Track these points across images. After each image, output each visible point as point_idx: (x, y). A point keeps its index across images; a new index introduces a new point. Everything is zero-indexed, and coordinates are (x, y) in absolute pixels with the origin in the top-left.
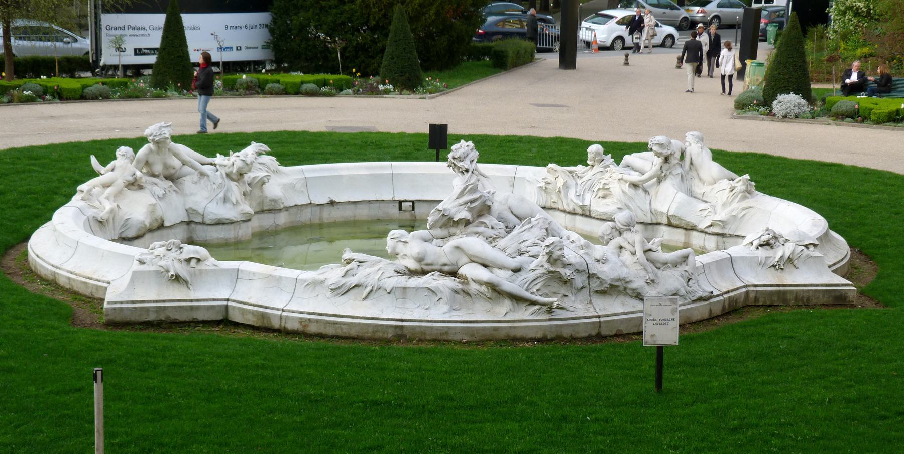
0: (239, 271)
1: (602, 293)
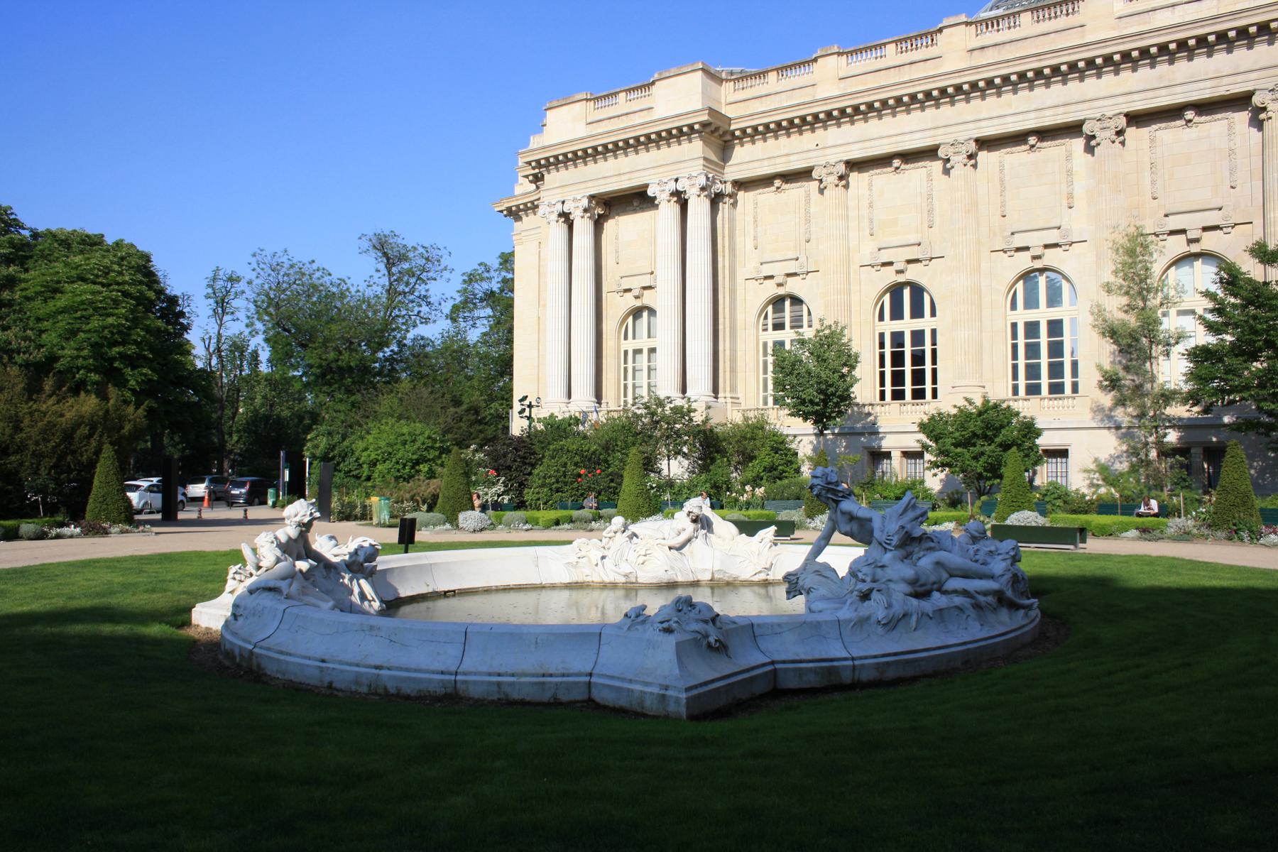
0: (755, 627)
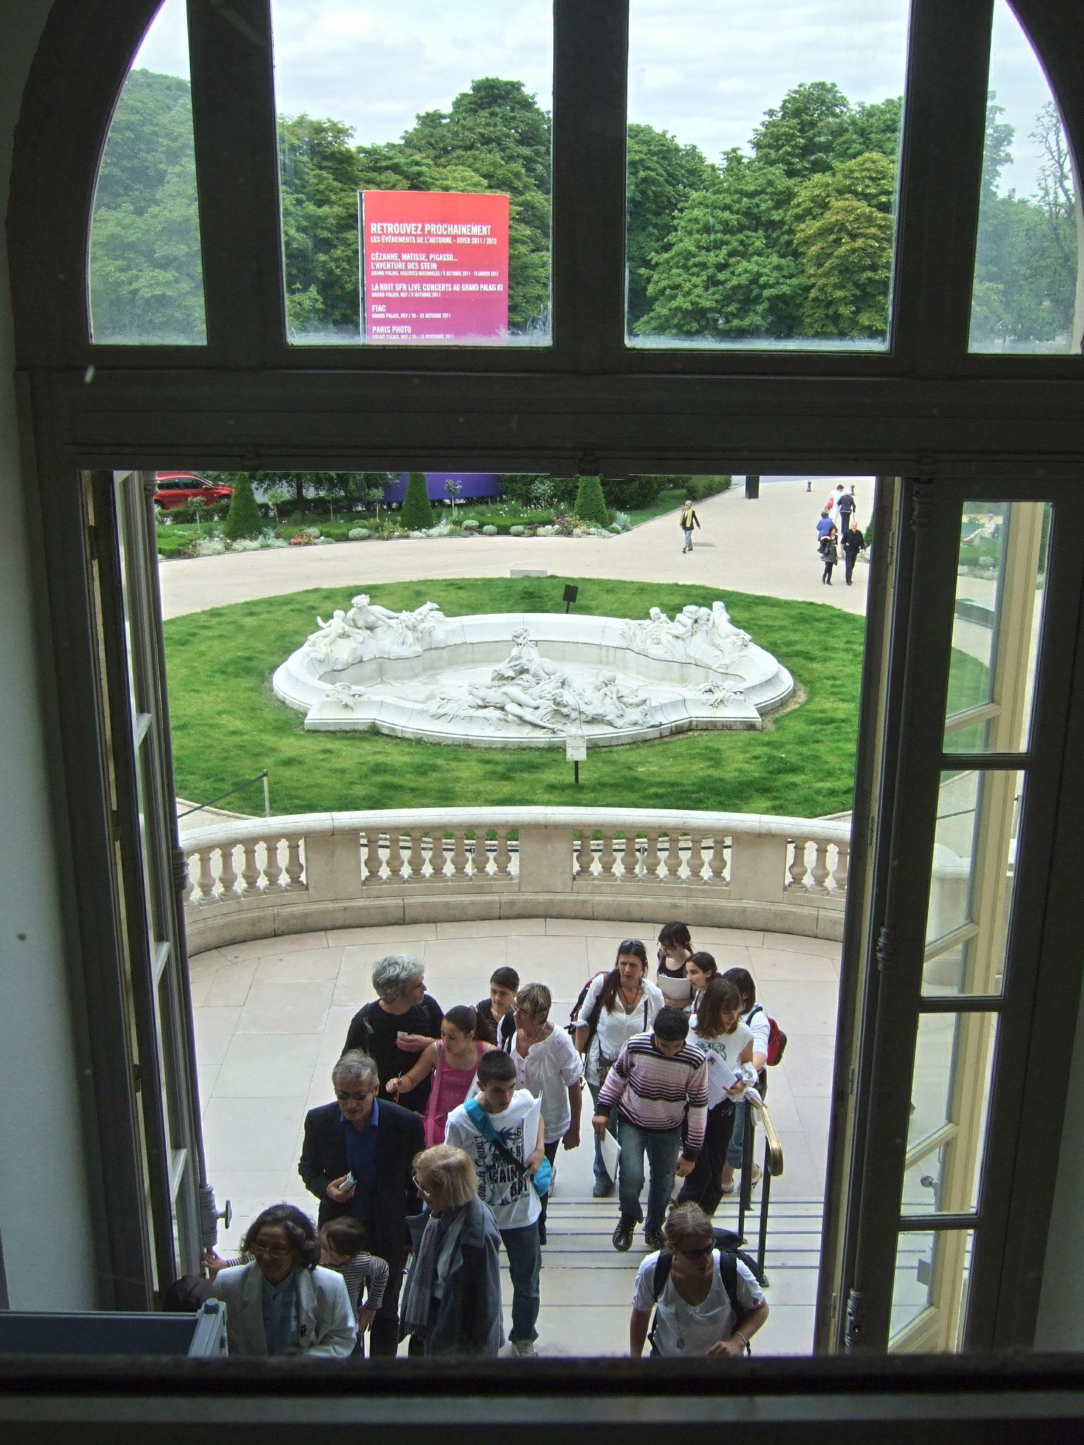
1: (588, 722)
